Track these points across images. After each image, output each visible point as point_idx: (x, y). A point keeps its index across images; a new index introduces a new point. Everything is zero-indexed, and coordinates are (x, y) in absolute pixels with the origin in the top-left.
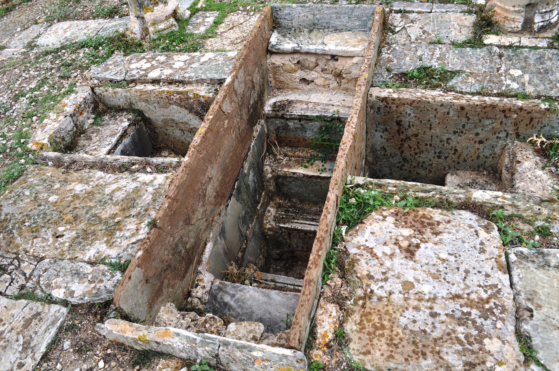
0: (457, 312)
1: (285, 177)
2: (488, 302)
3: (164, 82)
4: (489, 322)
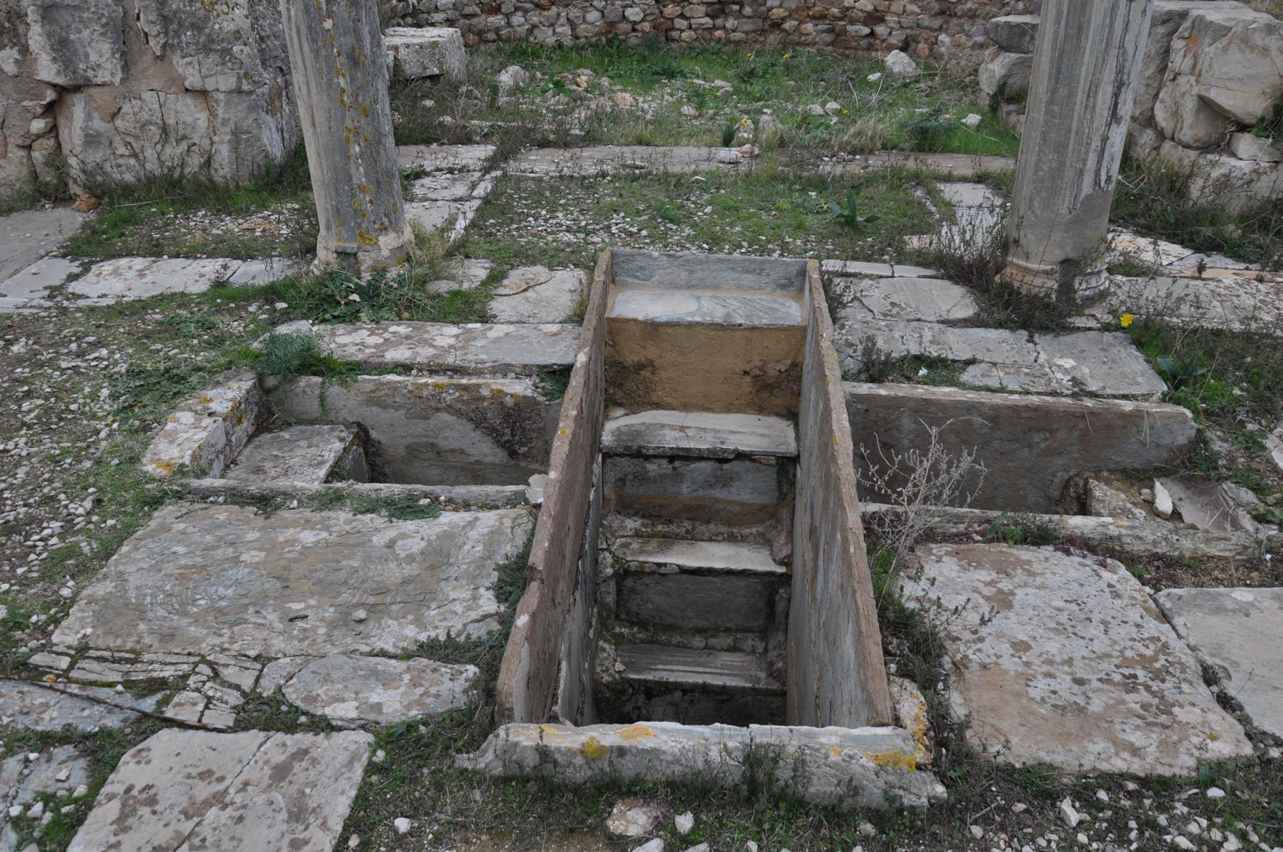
0: (1114, 675)
1: (640, 572)
2: (1156, 660)
3: (420, 370)
4: (1168, 685)
